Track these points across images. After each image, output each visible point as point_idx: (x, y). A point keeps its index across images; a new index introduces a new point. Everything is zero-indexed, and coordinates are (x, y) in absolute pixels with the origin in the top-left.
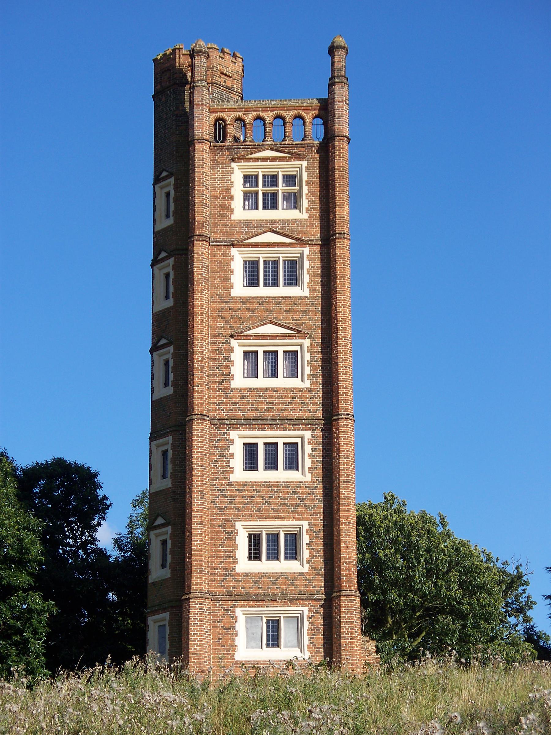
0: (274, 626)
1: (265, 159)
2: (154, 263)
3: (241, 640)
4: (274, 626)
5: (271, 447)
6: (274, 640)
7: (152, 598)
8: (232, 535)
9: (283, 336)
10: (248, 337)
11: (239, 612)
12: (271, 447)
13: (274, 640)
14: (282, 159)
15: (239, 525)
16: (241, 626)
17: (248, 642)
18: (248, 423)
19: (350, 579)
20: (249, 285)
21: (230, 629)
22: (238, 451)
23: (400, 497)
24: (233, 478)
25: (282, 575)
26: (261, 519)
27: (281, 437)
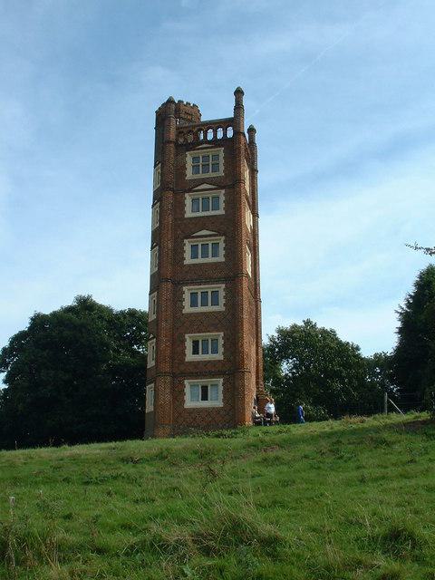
0: (205, 389)
1: (202, 149)
2: (152, 248)
3: (187, 397)
4: (205, 389)
5: (204, 294)
6: (205, 397)
7: (149, 376)
8: (183, 341)
9: (210, 236)
10: (193, 237)
11: (186, 382)
12: (204, 294)
13: (205, 397)
14: (212, 147)
15: (187, 336)
16: (187, 390)
17: (192, 397)
18: (193, 283)
19: (261, 368)
20: (194, 353)
21: (182, 393)
22: (189, 345)
23: (314, 321)
24: (186, 262)
25: (209, 362)
26: (199, 332)
27: (209, 288)
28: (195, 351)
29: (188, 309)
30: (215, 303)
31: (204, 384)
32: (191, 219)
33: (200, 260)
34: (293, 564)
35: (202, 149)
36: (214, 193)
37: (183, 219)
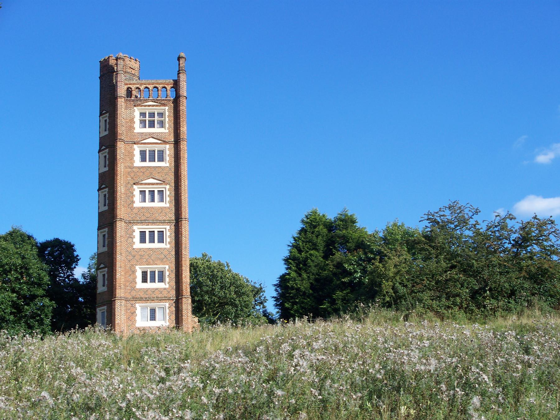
1: (149, 106)
3: (138, 318)
7: (99, 300)
8: (134, 272)
9: (157, 184)
10: (142, 184)
12: (153, 273)
14: (157, 106)
15: (137, 267)
16: (138, 311)
18: (142, 222)
20: (142, 161)
21: (134, 313)
22: (137, 235)
26: (148, 264)
27: (156, 228)
28: (144, 280)
29: (137, 245)
30: (161, 240)
31: (153, 307)
32: (139, 168)
33: (148, 204)
34: (552, 409)
35: (146, 106)
36: (161, 147)
37: (132, 208)
